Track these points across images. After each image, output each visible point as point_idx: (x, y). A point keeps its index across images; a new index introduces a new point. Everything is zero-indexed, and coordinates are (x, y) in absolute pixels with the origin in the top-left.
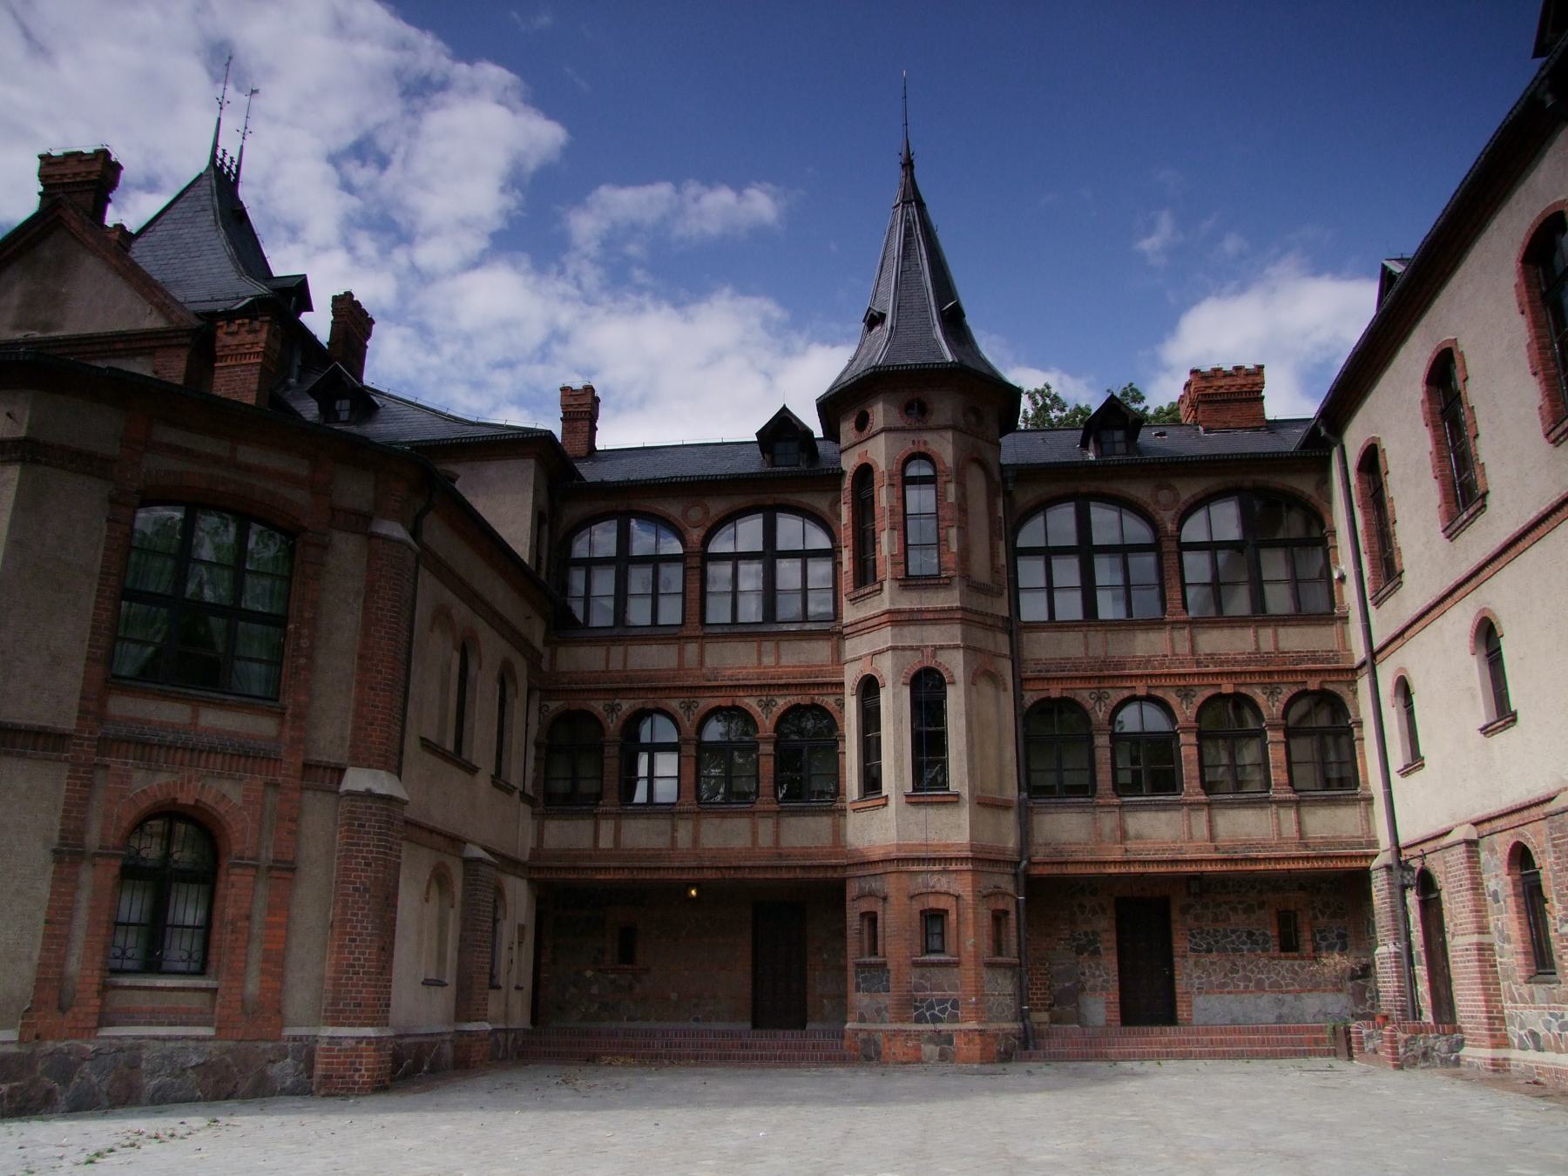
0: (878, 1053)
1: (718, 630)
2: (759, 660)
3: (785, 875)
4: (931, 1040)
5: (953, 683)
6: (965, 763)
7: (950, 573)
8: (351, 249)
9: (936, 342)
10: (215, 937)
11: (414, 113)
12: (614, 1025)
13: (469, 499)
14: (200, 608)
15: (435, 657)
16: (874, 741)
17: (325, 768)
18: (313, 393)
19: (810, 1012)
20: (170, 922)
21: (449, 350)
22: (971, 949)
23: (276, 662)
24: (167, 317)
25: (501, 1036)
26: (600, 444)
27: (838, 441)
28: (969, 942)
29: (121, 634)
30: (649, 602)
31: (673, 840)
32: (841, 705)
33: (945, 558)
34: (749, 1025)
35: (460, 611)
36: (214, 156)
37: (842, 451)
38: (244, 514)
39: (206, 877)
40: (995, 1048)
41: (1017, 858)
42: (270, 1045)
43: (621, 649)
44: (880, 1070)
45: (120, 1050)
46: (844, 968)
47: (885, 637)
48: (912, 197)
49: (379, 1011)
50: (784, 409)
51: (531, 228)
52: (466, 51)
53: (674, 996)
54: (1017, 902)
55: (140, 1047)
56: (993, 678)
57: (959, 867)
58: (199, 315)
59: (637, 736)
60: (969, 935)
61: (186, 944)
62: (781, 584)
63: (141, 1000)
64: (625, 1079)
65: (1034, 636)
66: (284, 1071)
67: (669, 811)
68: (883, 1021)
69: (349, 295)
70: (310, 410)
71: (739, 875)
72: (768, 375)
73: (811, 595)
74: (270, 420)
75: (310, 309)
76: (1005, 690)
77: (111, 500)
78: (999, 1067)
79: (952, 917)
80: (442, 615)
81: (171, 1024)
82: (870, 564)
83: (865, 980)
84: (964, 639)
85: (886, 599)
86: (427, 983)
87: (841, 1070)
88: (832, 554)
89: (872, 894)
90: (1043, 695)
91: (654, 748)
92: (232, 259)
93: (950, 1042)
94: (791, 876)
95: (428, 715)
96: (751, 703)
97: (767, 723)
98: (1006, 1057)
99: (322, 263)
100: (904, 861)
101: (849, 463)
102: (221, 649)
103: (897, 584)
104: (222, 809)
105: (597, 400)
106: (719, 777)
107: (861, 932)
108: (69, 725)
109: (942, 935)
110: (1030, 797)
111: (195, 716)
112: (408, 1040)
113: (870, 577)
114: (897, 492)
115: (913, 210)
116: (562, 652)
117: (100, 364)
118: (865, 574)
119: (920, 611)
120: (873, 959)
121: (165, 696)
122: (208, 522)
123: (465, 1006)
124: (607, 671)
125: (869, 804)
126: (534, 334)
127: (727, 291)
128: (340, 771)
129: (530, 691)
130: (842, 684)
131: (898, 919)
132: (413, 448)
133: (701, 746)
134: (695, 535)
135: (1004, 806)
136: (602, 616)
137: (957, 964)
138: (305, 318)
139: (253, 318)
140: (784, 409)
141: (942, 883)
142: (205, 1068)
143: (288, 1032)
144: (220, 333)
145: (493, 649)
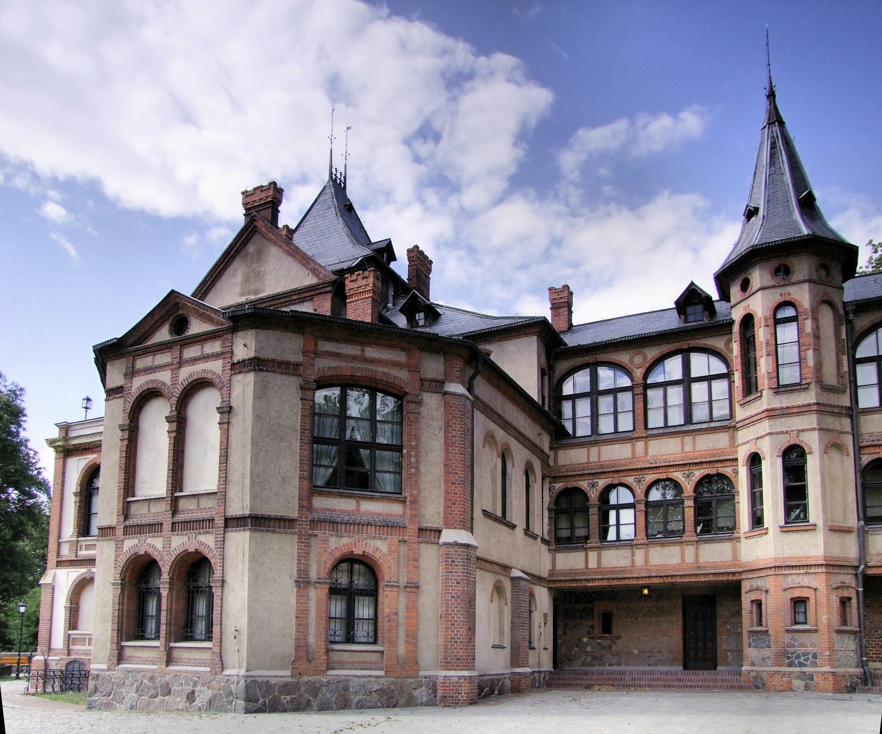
0: (764, 685)
1: (656, 432)
2: (682, 448)
3: (702, 579)
4: (798, 677)
5: (811, 453)
6: (820, 505)
7: (808, 381)
8: (421, 201)
9: (795, 221)
10: (380, 624)
11: (454, 99)
12: (601, 668)
13: (499, 365)
14: (353, 446)
15: (487, 463)
16: (758, 494)
17: (431, 530)
18: (402, 311)
19: (719, 660)
20: (356, 616)
21: (488, 261)
22: (825, 621)
23: (398, 471)
24: (317, 276)
25: (536, 675)
26: (574, 323)
27: (729, 300)
28: (824, 618)
29: (315, 462)
30: (612, 417)
31: (633, 561)
32: (736, 473)
33: (804, 371)
34: (681, 668)
35: (500, 434)
36: (331, 173)
37: (732, 307)
38: (372, 388)
39: (373, 593)
40: (844, 683)
41: (856, 564)
42: (413, 680)
43: (596, 449)
44: (763, 694)
45: (339, 682)
46: (741, 634)
47: (765, 426)
48: (775, 119)
49: (469, 661)
50: (692, 284)
51: (535, 170)
52: (484, 48)
53: (636, 652)
54: (858, 592)
55: (348, 681)
56: (838, 447)
57: (816, 570)
58: (335, 273)
59: (608, 501)
60: (824, 612)
61: (366, 628)
62: (694, 399)
63: (346, 657)
64: (608, 699)
65: (869, 417)
66: (422, 693)
67: (630, 544)
68: (766, 666)
69: (416, 247)
70: (401, 321)
71: (674, 580)
72: (696, 251)
73: (714, 404)
74: (379, 331)
75: (395, 259)
76: (848, 455)
77: (302, 388)
78: (848, 696)
79: (812, 602)
80: (490, 438)
81: (362, 669)
82: (753, 380)
83: (754, 641)
84: (819, 423)
85: (766, 400)
86: (494, 647)
87: (740, 694)
88: (728, 376)
89: (758, 589)
90: (875, 456)
91: (619, 507)
92: (348, 236)
93: (812, 679)
94: (706, 579)
95: (486, 497)
96: (678, 475)
97: (688, 487)
98: (852, 689)
99: (399, 226)
100: (781, 568)
101: (737, 315)
102: (368, 467)
103: (772, 392)
104: (377, 555)
105: (571, 294)
106: (658, 522)
107: (751, 612)
108: (295, 514)
109: (805, 613)
110: (866, 524)
111: (358, 506)
112: (486, 678)
113: (753, 389)
114: (770, 330)
115: (776, 128)
116: (561, 453)
117: (285, 309)
118: (750, 387)
119: (788, 408)
120: (759, 628)
121: (341, 496)
122: (353, 394)
123: (516, 658)
124: (589, 463)
125: (755, 533)
126: (541, 242)
127: (666, 192)
128: (439, 532)
129: (543, 478)
130: (737, 459)
131: (776, 605)
132: (464, 338)
133: (648, 504)
134: (639, 373)
135: (848, 531)
136: (583, 429)
137: (816, 631)
138: (393, 265)
139: (365, 270)
140: (692, 284)
141: (805, 581)
142: (381, 691)
143: (422, 673)
144: (347, 282)
145: (520, 455)
